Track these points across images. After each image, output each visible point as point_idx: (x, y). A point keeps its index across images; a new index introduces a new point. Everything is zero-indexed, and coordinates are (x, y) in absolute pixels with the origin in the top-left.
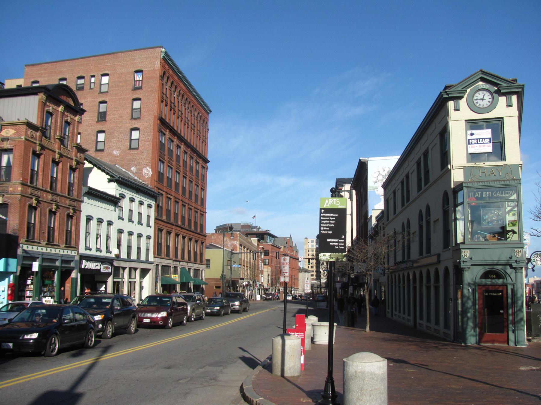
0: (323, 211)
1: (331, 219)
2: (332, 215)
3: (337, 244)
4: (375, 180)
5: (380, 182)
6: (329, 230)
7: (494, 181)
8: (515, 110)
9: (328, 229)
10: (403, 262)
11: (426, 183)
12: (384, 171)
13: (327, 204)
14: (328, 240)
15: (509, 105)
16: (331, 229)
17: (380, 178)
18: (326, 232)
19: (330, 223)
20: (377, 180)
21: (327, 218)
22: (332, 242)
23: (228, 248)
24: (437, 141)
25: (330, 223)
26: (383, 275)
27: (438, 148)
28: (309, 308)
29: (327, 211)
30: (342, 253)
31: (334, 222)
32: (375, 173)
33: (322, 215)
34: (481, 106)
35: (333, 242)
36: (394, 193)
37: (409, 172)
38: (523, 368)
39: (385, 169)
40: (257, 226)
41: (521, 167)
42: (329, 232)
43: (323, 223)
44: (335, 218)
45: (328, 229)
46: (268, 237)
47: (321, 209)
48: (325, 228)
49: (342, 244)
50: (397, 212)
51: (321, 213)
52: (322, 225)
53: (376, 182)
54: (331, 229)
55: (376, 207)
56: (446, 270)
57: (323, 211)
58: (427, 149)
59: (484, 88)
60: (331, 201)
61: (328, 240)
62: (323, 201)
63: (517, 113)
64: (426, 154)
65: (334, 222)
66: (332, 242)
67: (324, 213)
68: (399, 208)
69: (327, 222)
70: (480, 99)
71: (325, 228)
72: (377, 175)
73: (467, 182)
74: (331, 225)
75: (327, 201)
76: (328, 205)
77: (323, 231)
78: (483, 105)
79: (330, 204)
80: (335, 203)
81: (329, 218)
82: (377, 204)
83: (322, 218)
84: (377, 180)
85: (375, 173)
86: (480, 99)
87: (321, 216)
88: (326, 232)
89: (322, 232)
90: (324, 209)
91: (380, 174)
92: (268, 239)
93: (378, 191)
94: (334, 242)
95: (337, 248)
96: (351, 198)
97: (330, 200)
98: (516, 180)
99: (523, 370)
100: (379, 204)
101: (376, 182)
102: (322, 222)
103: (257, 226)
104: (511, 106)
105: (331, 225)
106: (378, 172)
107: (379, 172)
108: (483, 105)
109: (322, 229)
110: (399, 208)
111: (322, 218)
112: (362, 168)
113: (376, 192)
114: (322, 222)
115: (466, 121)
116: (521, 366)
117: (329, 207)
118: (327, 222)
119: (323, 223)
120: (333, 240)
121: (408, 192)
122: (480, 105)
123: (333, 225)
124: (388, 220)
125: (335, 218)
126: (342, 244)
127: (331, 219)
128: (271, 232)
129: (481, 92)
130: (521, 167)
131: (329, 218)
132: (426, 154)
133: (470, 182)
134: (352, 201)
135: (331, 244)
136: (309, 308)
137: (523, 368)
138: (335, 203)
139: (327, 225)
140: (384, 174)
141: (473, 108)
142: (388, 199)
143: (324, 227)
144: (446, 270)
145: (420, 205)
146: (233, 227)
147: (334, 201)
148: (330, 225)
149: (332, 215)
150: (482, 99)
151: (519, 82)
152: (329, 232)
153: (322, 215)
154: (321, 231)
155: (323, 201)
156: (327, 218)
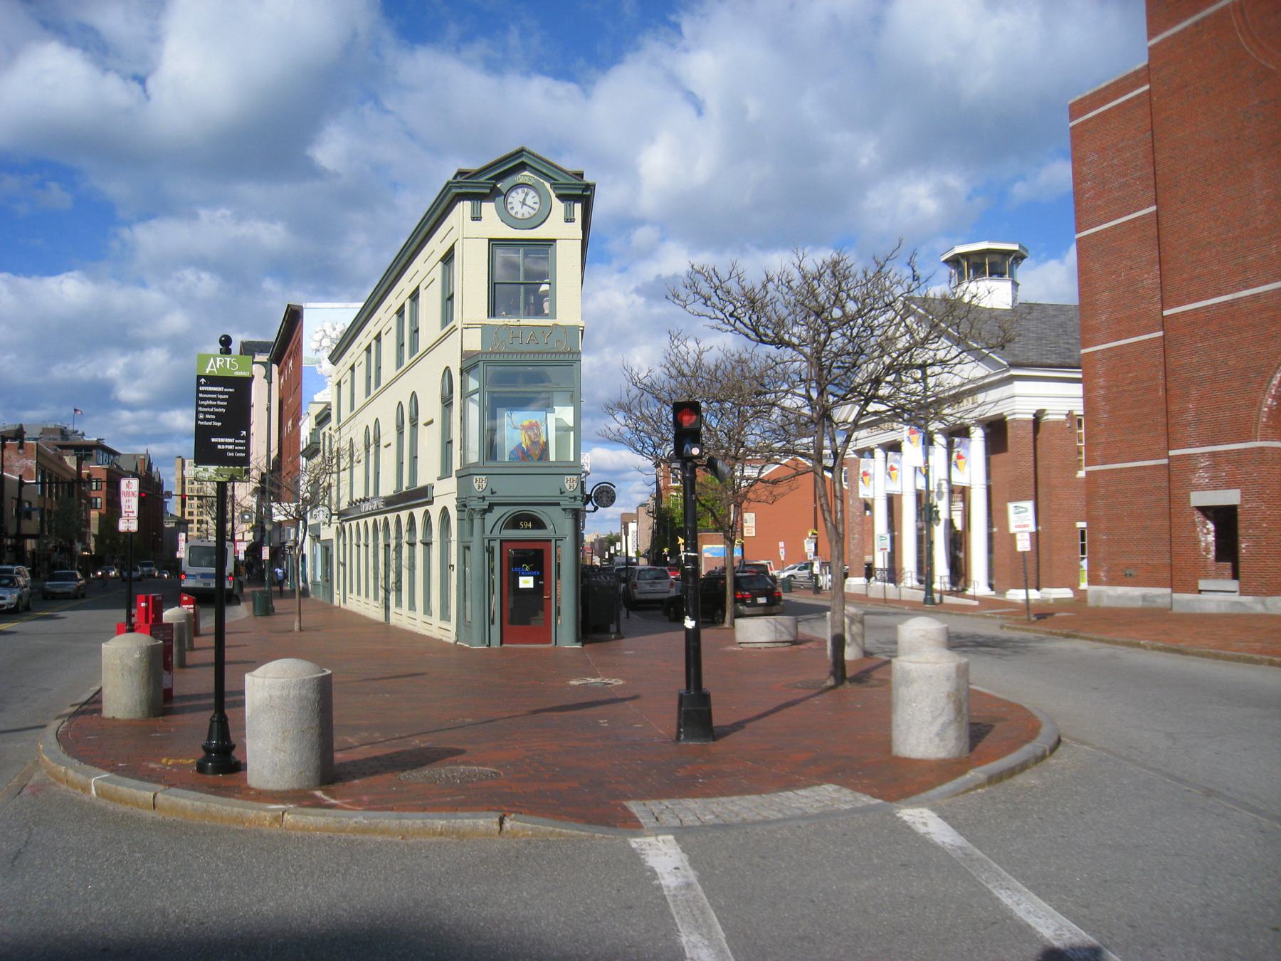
0: (203, 380)
1: (221, 397)
2: (221, 389)
3: (231, 447)
4: (314, 345)
5: (326, 349)
6: (216, 420)
7: (534, 353)
8: (576, 229)
9: (214, 417)
10: (365, 500)
11: (412, 352)
12: (334, 329)
13: (212, 367)
14: (213, 440)
15: (569, 220)
16: (219, 417)
17: (326, 342)
18: (210, 423)
19: (218, 406)
20: (321, 345)
21: (212, 396)
22: (221, 444)
23: (13, 474)
24: (438, 272)
25: (218, 406)
26: (327, 526)
27: (437, 287)
28: (915, 307)
29: (213, 380)
30: (241, 466)
31: (226, 403)
32: (317, 332)
33: (201, 389)
34: (519, 216)
35: (224, 443)
36: (352, 368)
37: (380, 332)
38: (574, 682)
39: (336, 326)
40: (77, 431)
41: (582, 331)
42: (215, 423)
43: (203, 406)
44: (227, 396)
45: (214, 417)
46: (101, 453)
47: (199, 377)
48: (207, 416)
49: (241, 448)
50: (357, 408)
51: (199, 384)
52: (200, 409)
53: (317, 350)
54: (219, 417)
55: (317, 398)
56: (445, 511)
57: (203, 380)
58: (418, 288)
59: (527, 182)
60: (221, 361)
61: (213, 440)
62: (204, 359)
63: (580, 235)
64: (415, 296)
65: (226, 403)
66: (221, 444)
67: (205, 385)
68: (360, 399)
69: (211, 402)
70: (525, 199)
71: (207, 416)
72: (321, 337)
73: (487, 353)
74: (220, 410)
75: (212, 360)
76: (215, 370)
77: (202, 420)
78: (523, 215)
79: (218, 367)
80: (228, 367)
81: (215, 396)
82: (319, 392)
83: (201, 395)
84: (321, 345)
85: (317, 332)
86: (525, 199)
87: (198, 392)
88: (210, 423)
89: (202, 423)
90: (205, 377)
91: (326, 335)
92: (100, 455)
93: (321, 367)
94: (225, 444)
95: (231, 457)
96: (268, 377)
97: (218, 359)
98: (574, 353)
99: (575, 686)
100: (323, 392)
101: (317, 350)
102: (202, 403)
103: (77, 431)
104: (572, 220)
105: (220, 410)
106: (322, 332)
107: (325, 331)
108: (523, 215)
109: (201, 416)
110: (360, 399)
111: (201, 395)
112: (293, 317)
113: (318, 369)
114: (202, 403)
115: (490, 240)
116: (571, 678)
117: (216, 373)
118: (211, 402)
119: (203, 406)
120: (222, 440)
121: (379, 368)
122: (517, 213)
123: (224, 410)
124: (339, 420)
125: (227, 396)
126: (241, 448)
127: (221, 397)
128: (107, 444)
129: (520, 191)
130: (582, 331)
131: (215, 396)
132: (415, 296)
133: (491, 353)
134: (270, 383)
135: (219, 447)
136: (915, 307)
137: (574, 682)
138: (228, 367)
139: (212, 410)
140: (334, 336)
141: (507, 217)
142: (340, 381)
143: (205, 413)
144: (445, 511)
145: (400, 392)
146: (25, 430)
147: (226, 361)
148: (217, 410)
149: (221, 389)
150: (524, 203)
151: (588, 179)
152: (215, 423)
153: (201, 389)
154: (199, 422)
155: (204, 359)
156: (212, 396)
